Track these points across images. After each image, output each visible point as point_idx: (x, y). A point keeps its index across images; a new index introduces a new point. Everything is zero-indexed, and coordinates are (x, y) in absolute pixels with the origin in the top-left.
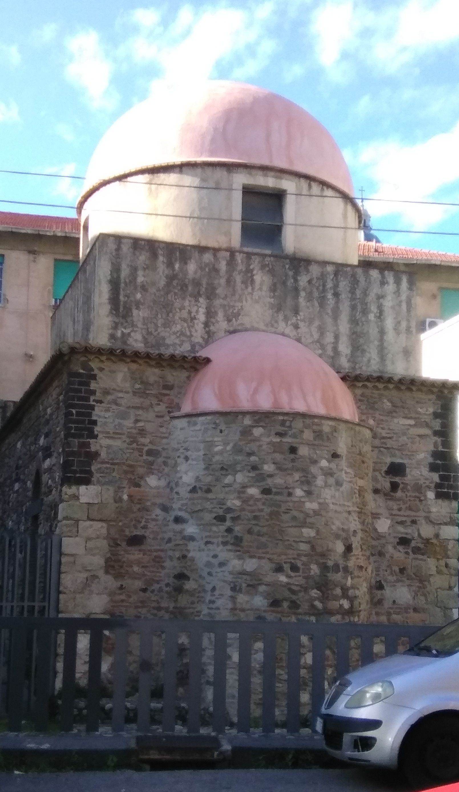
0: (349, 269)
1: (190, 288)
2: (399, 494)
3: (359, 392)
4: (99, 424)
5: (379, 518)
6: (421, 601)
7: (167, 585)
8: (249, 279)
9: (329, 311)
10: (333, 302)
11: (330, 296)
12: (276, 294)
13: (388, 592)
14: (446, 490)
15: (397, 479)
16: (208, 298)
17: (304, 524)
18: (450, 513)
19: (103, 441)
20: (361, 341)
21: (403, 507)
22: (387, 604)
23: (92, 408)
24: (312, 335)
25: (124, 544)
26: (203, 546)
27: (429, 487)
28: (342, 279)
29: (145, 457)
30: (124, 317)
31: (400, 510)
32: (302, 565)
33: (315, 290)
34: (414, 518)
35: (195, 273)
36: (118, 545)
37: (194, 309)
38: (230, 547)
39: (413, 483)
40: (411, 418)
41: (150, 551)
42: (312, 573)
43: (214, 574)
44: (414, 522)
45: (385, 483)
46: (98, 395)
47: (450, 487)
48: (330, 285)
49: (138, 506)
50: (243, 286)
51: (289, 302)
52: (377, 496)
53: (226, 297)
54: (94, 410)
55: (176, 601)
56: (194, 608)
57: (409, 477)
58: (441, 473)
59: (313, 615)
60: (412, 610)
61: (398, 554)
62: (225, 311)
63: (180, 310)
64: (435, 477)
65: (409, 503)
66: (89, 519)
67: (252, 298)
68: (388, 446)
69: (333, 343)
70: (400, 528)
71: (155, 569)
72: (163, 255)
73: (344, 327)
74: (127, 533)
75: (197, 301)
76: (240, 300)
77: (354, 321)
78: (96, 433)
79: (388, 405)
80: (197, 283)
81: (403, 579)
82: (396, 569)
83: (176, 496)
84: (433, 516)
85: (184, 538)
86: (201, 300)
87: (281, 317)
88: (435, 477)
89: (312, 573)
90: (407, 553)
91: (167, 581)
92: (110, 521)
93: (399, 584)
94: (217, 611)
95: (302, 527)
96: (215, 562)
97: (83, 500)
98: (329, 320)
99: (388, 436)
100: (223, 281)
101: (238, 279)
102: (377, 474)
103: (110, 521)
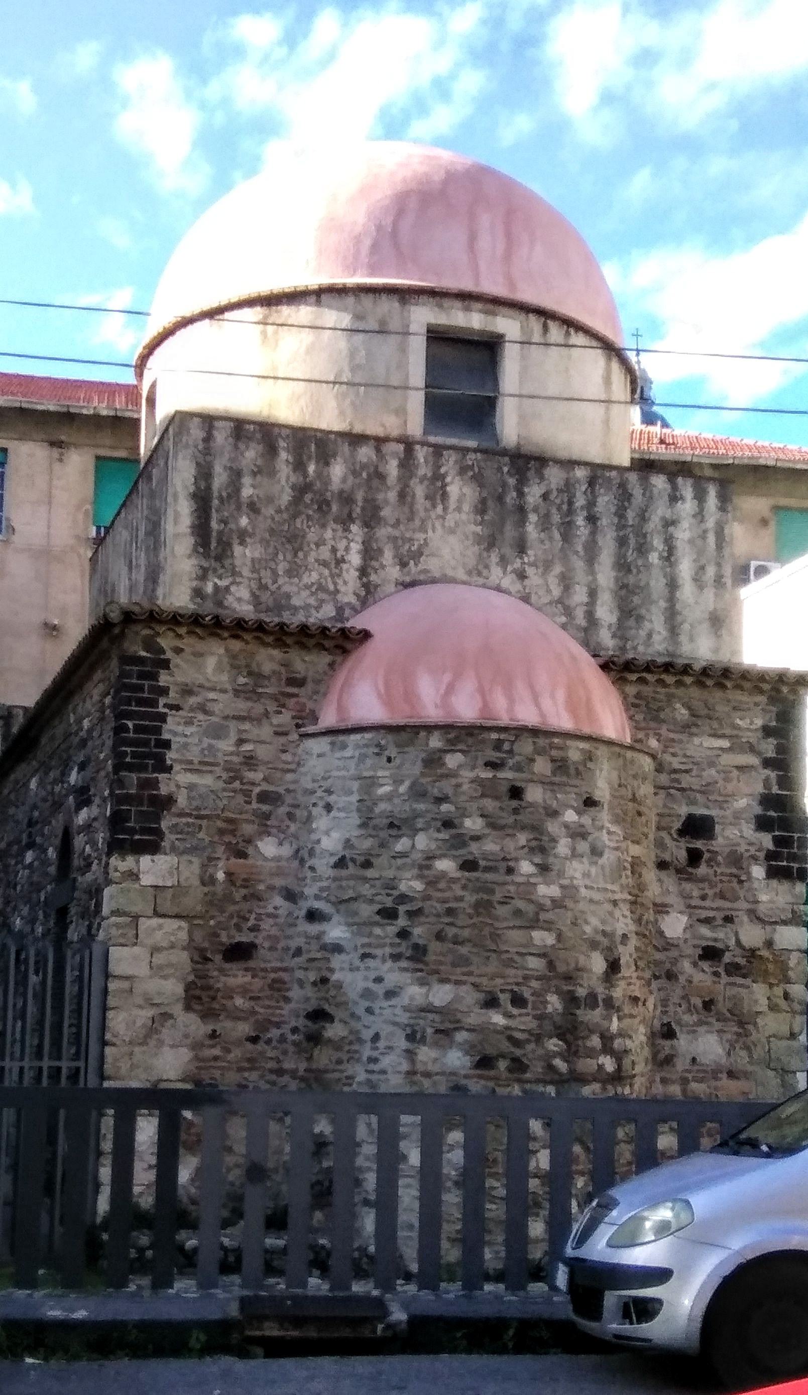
0: (614, 473)
1: (335, 508)
2: (702, 870)
3: (631, 690)
4: (173, 746)
5: (667, 913)
6: (741, 1059)
7: (295, 1030)
8: (438, 492)
9: (580, 548)
10: (587, 532)
11: (580, 521)
12: (486, 518)
13: (683, 1042)
14: (785, 863)
15: (699, 844)
16: (367, 525)
17: (534, 924)
18: (793, 904)
19: (183, 778)
20: (636, 600)
21: (710, 892)
22: (681, 1064)
23: (163, 718)
24: (549, 591)
25: (218, 958)
26: (357, 962)
27: (754, 858)
28: (602, 491)
29: (255, 805)
30: (219, 558)
31: (703, 898)
32: (532, 995)
33: (554, 511)
34: (728, 913)
35: (344, 480)
36: (207, 960)
37: (341, 545)
38: (404, 964)
39: (727, 850)
40: (723, 736)
41: (264, 970)
42: (550, 1009)
43: (377, 1011)
44: (728, 919)
45: (678, 851)
46: (173, 696)
47: (793, 858)
48: (580, 501)
49: (243, 891)
50: (428, 504)
51: (510, 532)
52: (663, 874)
53: (398, 522)
54: (165, 721)
55: (310, 1059)
56: (342, 1071)
57: (720, 840)
58: (777, 833)
59: (551, 1082)
60: (725, 1075)
61: (701, 977)
62: (396, 548)
63: (318, 545)
64: (767, 840)
65: (720, 885)
66: (157, 914)
67: (443, 526)
68: (684, 785)
69: (587, 604)
70: (705, 931)
71: (273, 1003)
72: (287, 450)
73: (606, 576)
74: (224, 938)
75: (347, 530)
76: (423, 529)
77: (623, 566)
78: (169, 762)
79: (682, 713)
80: (346, 499)
81: (710, 1019)
82: (697, 1002)
83: (309, 874)
84: (762, 909)
85: (324, 947)
86: (354, 528)
87: (494, 558)
88: (767, 840)
89: (550, 1009)
90: (716, 974)
91: (293, 1023)
92: (195, 917)
93: (702, 1029)
94: (382, 1077)
95: (532, 928)
96: (379, 989)
97: (147, 880)
98: (579, 564)
99: (683, 767)
100: (392, 496)
101: (420, 491)
102: (664, 834)
103: (195, 917)
